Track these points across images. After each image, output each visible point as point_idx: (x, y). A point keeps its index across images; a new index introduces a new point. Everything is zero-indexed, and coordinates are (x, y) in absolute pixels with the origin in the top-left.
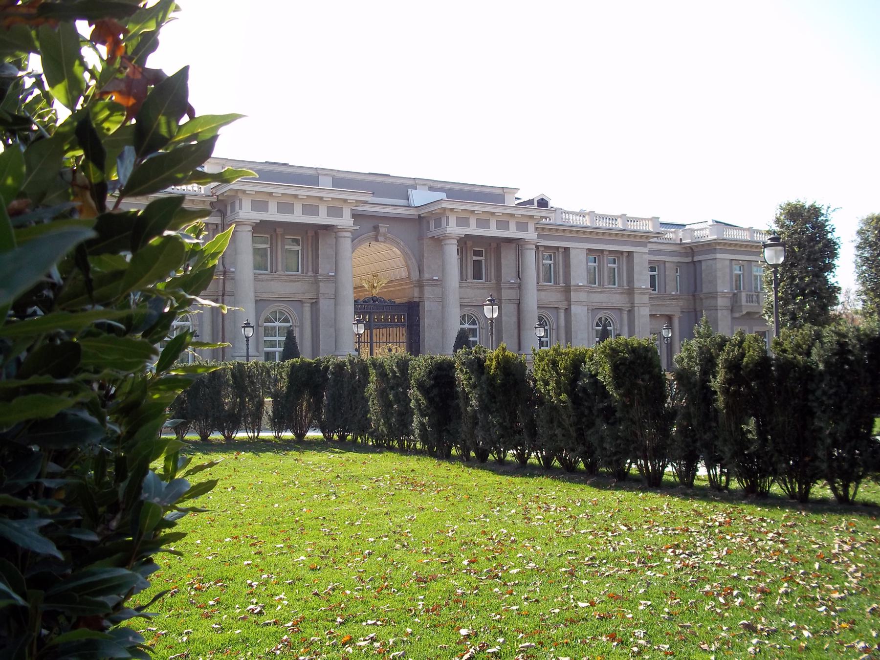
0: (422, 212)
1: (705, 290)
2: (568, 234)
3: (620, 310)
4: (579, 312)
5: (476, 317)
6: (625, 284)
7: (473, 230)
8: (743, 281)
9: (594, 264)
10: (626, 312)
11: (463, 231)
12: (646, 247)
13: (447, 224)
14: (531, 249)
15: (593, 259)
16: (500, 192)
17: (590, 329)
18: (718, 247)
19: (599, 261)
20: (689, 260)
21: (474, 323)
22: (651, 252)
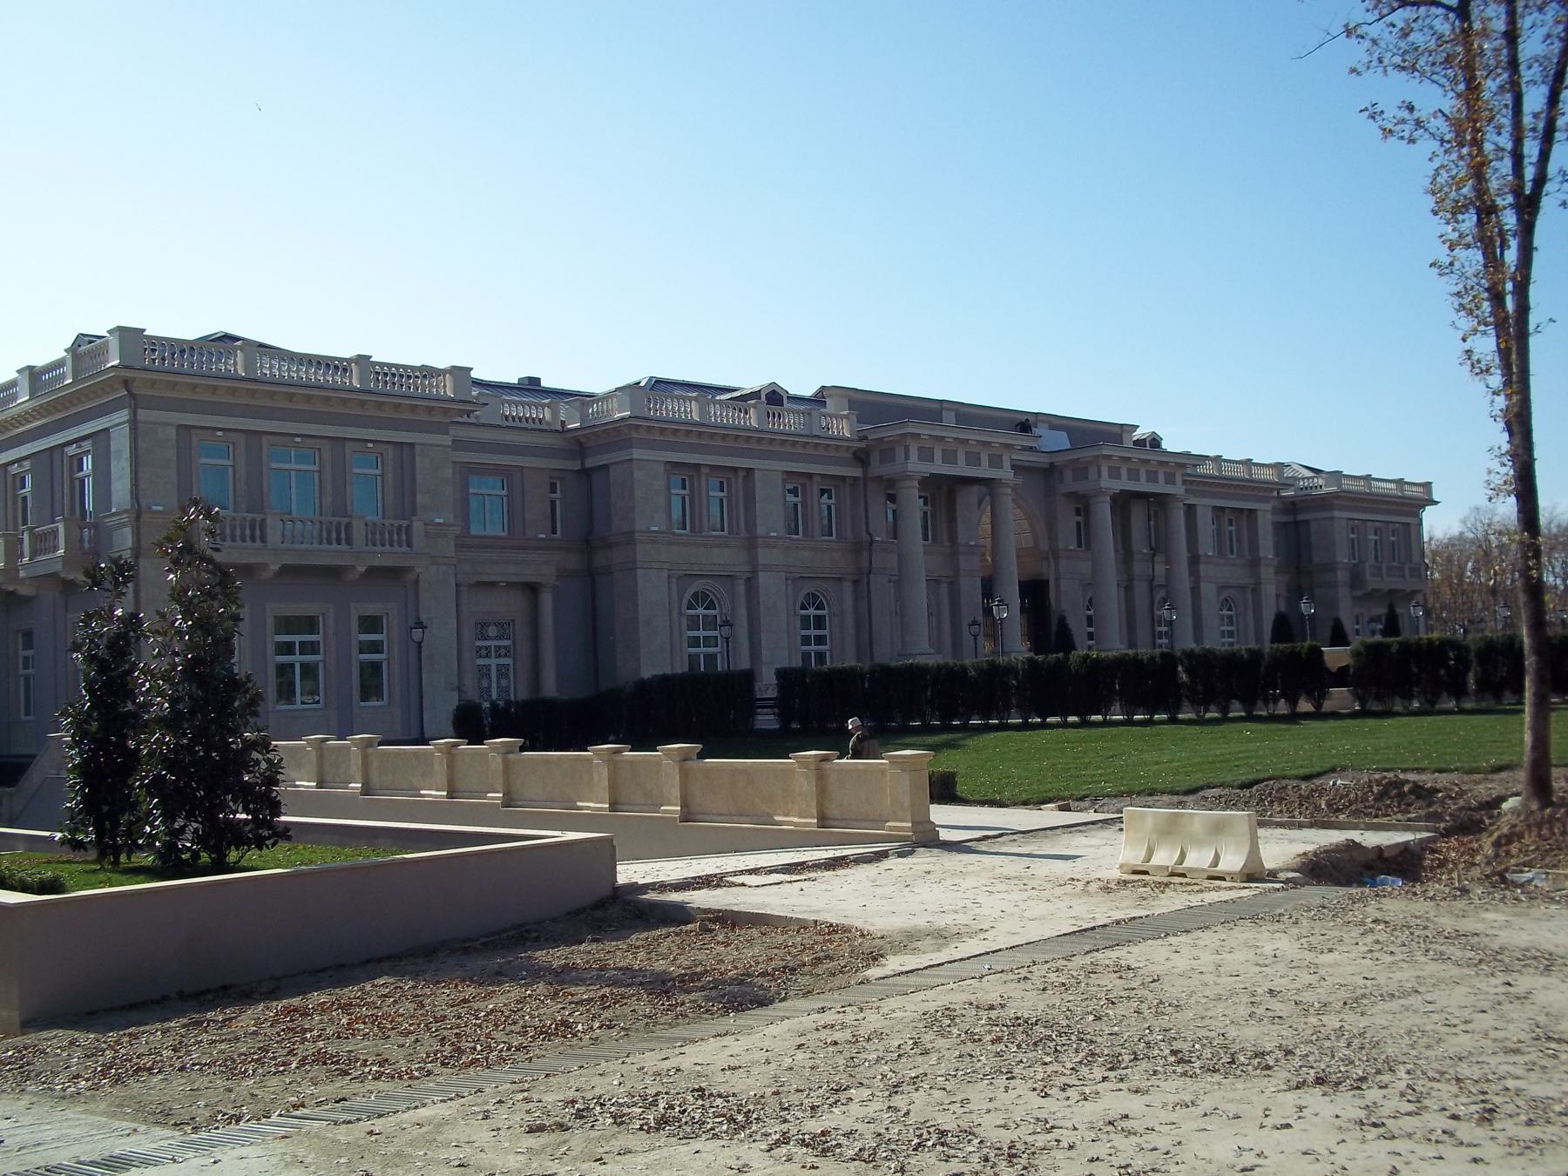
0: (1057, 459)
1: (1316, 560)
2: (777, 448)
3: (1243, 588)
4: (772, 587)
5: (715, 596)
6: (1247, 553)
7: (939, 467)
8: (1359, 549)
9: (721, 494)
10: (742, 582)
11: (927, 469)
12: (447, 433)
13: (907, 458)
14: (912, 487)
15: (680, 481)
16: (1118, 430)
17: (675, 613)
18: (1336, 502)
19: (692, 485)
20: (576, 465)
21: (711, 606)
22: (458, 445)
